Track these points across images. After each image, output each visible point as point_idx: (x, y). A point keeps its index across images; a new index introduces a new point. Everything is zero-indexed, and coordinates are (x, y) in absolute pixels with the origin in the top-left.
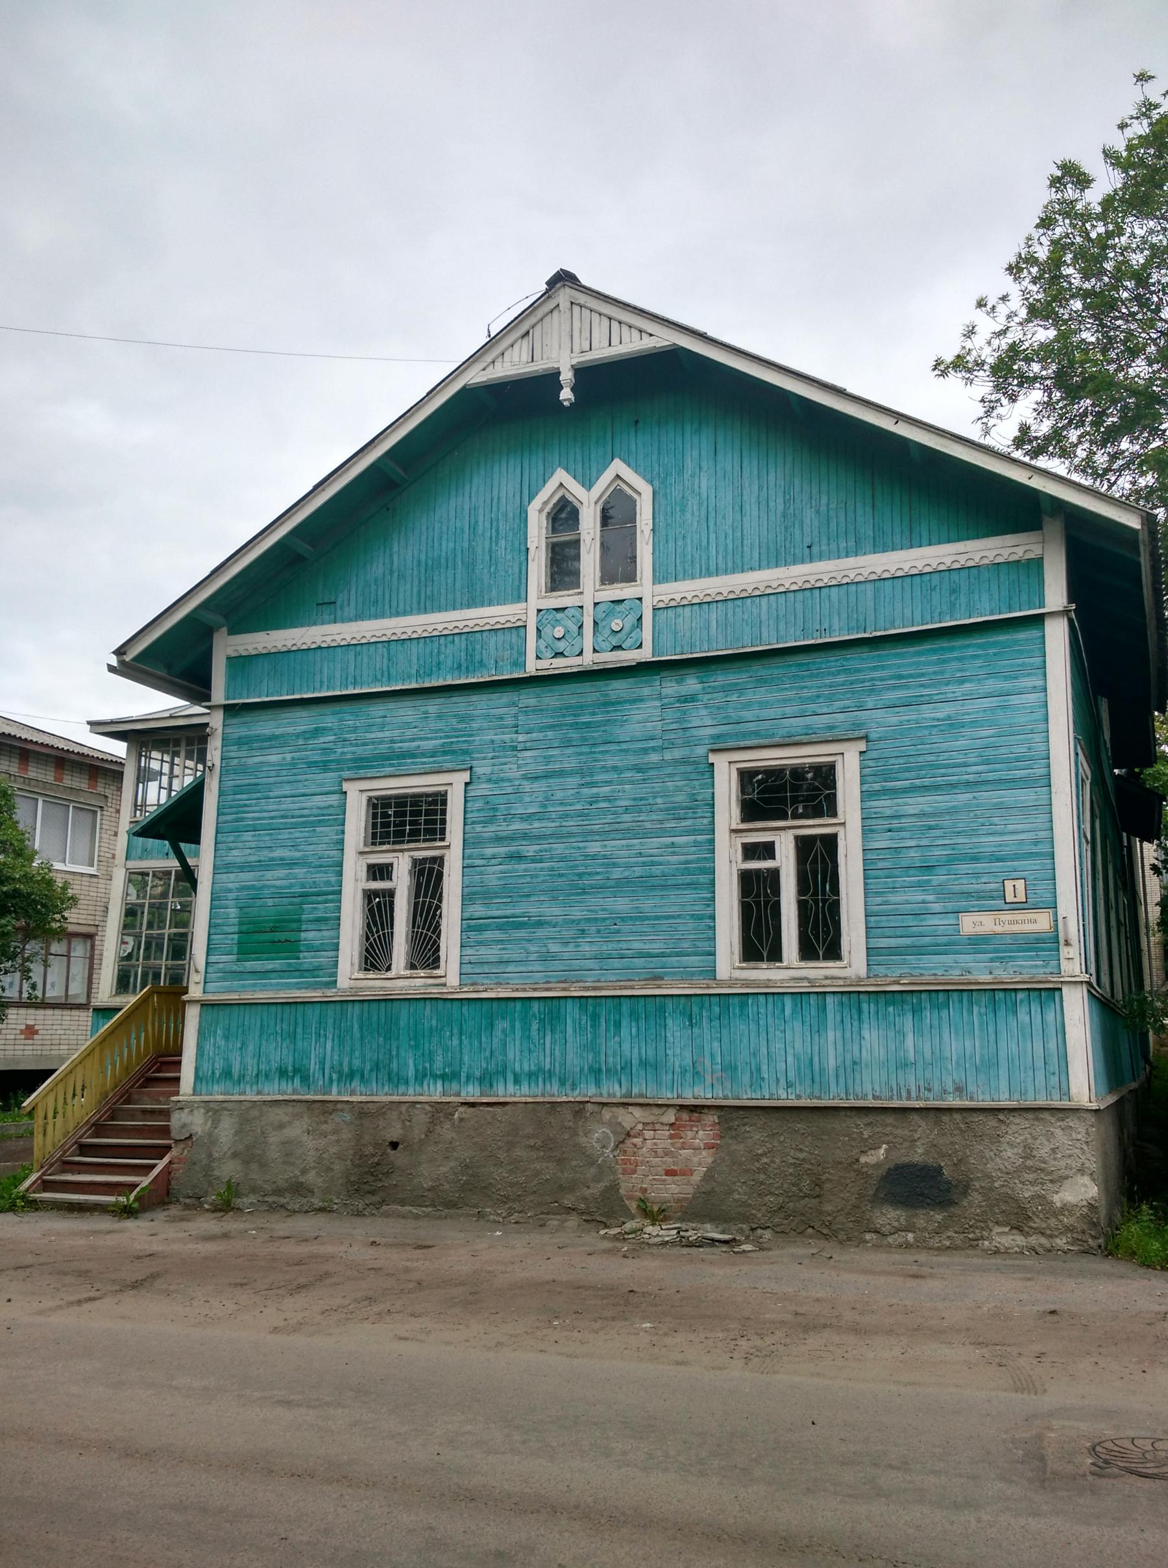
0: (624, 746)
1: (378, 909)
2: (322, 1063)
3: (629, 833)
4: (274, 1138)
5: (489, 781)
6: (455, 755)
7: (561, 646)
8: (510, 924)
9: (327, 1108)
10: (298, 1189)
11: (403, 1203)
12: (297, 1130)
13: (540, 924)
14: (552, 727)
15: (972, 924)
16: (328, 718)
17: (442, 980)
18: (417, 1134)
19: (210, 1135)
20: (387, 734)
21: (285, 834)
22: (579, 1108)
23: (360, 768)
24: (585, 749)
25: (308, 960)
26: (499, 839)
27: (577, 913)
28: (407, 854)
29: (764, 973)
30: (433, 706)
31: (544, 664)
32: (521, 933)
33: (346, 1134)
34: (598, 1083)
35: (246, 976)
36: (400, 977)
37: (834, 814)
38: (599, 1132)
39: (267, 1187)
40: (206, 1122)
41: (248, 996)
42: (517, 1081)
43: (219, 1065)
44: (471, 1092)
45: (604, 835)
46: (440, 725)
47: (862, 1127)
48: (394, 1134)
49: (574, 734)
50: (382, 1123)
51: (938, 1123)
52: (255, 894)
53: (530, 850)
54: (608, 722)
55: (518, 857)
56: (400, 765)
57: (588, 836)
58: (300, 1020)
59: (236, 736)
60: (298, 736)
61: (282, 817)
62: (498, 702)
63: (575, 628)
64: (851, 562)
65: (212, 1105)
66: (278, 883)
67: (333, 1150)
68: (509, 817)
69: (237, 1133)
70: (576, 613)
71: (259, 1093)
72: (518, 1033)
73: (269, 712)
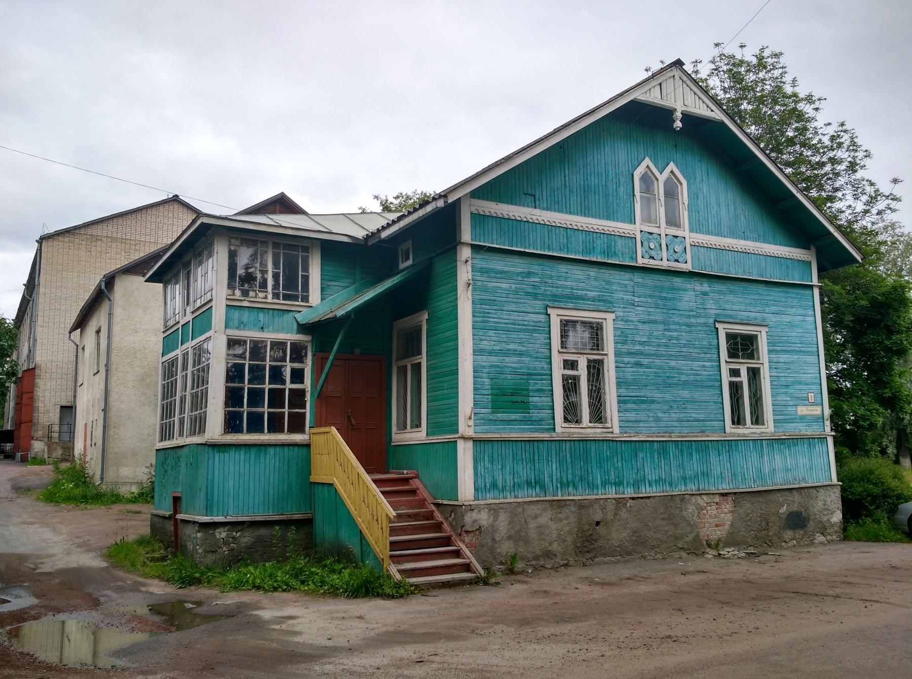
0: (681, 312)
1: (571, 386)
2: (551, 477)
3: (686, 358)
4: (532, 525)
5: (622, 320)
6: (605, 303)
7: (653, 253)
8: (640, 401)
9: (560, 504)
10: (548, 554)
11: (605, 555)
12: (545, 518)
13: (653, 402)
14: (650, 296)
15: (802, 410)
16: (535, 266)
17: (610, 430)
18: (610, 516)
19: (492, 526)
20: (569, 283)
21: (514, 335)
22: (682, 497)
23: (554, 301)
24: (665, 311)
25: (535, 414)
26: (630, 354)
27: (668, 397)
28: (746, 365)
29: (741, 430)
30: (593, 272)
31: (646, 261)
32: (644, 406)
33: (573, 519)
34: (685, 484)
35: (498, 423)
36: (587, 428)
37: (758, 359)
38: (691, 508)
39: (530, 556)
40: (489, 517)
41: (506, 436)
42: (650, 485)
43: (489, 480)
44: (629, 492)
45: (676, 358)
46: (596, 284)
47: (779, 498)
48: (598, 517)
49: (660, 302)
50: (591, 511)
51: (801, 494)
52: (500, 371)
53: (645, 361)
54: (674, 299)
55: (638, 364)
56: (576, 303)
57: (670, 357)
58: (536, 451)
59: (479, 266)
60: (518, 274)
61: (512, 324)
62: (626, 276)
63: (658, 245)
64: (758, 244)
65: (493, 506)
66: (514, 365)
67: (566, 529)
68: (634, 342)
69: (509, 524)
70: (658, 237)
71: (516, 497)
72: (649, 459)
73: (499, 255)
